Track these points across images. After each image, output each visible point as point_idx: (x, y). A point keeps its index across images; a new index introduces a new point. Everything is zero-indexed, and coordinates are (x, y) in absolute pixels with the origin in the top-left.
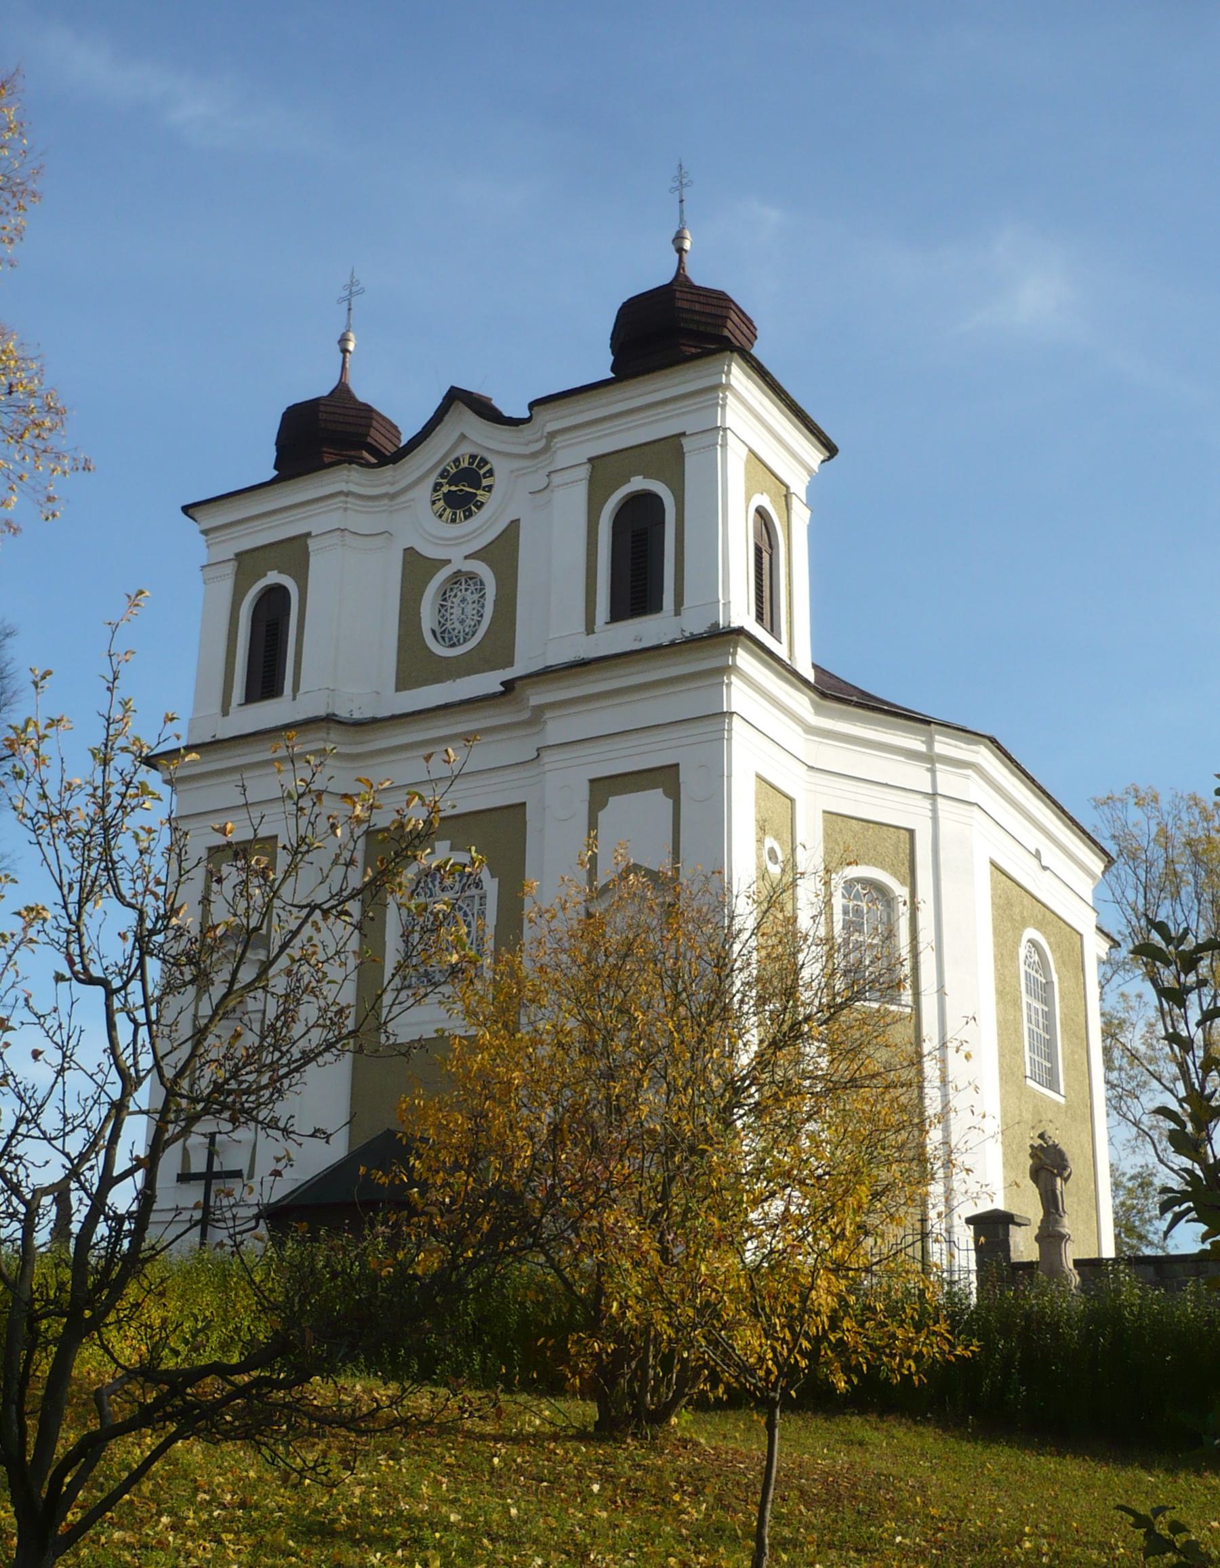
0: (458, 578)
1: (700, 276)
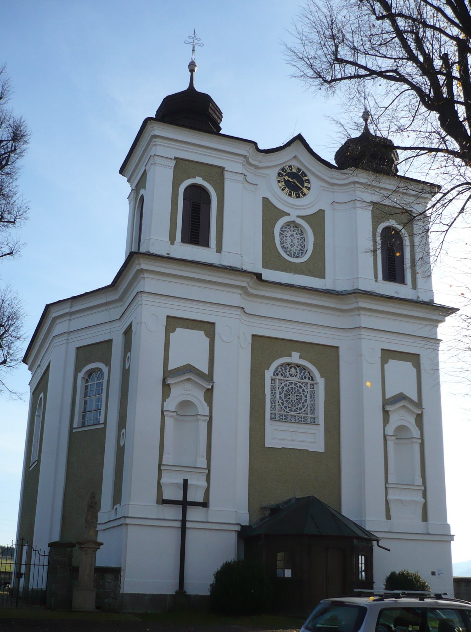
0: (292, 225)
1: (199, 88)
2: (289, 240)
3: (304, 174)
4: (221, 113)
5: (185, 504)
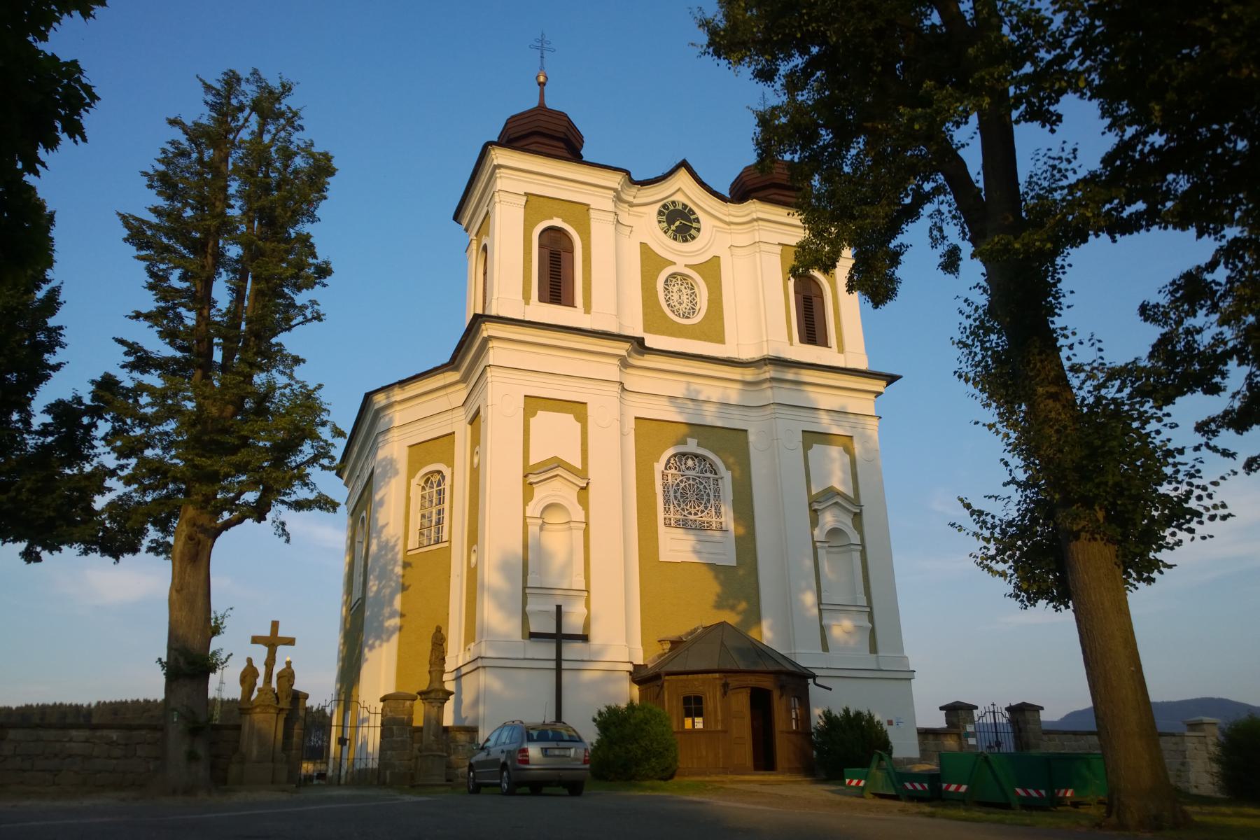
1: (551, 104)
2: (676, 297)
3: (692, 212)
4: (581, 137)
5: (559, 637)
